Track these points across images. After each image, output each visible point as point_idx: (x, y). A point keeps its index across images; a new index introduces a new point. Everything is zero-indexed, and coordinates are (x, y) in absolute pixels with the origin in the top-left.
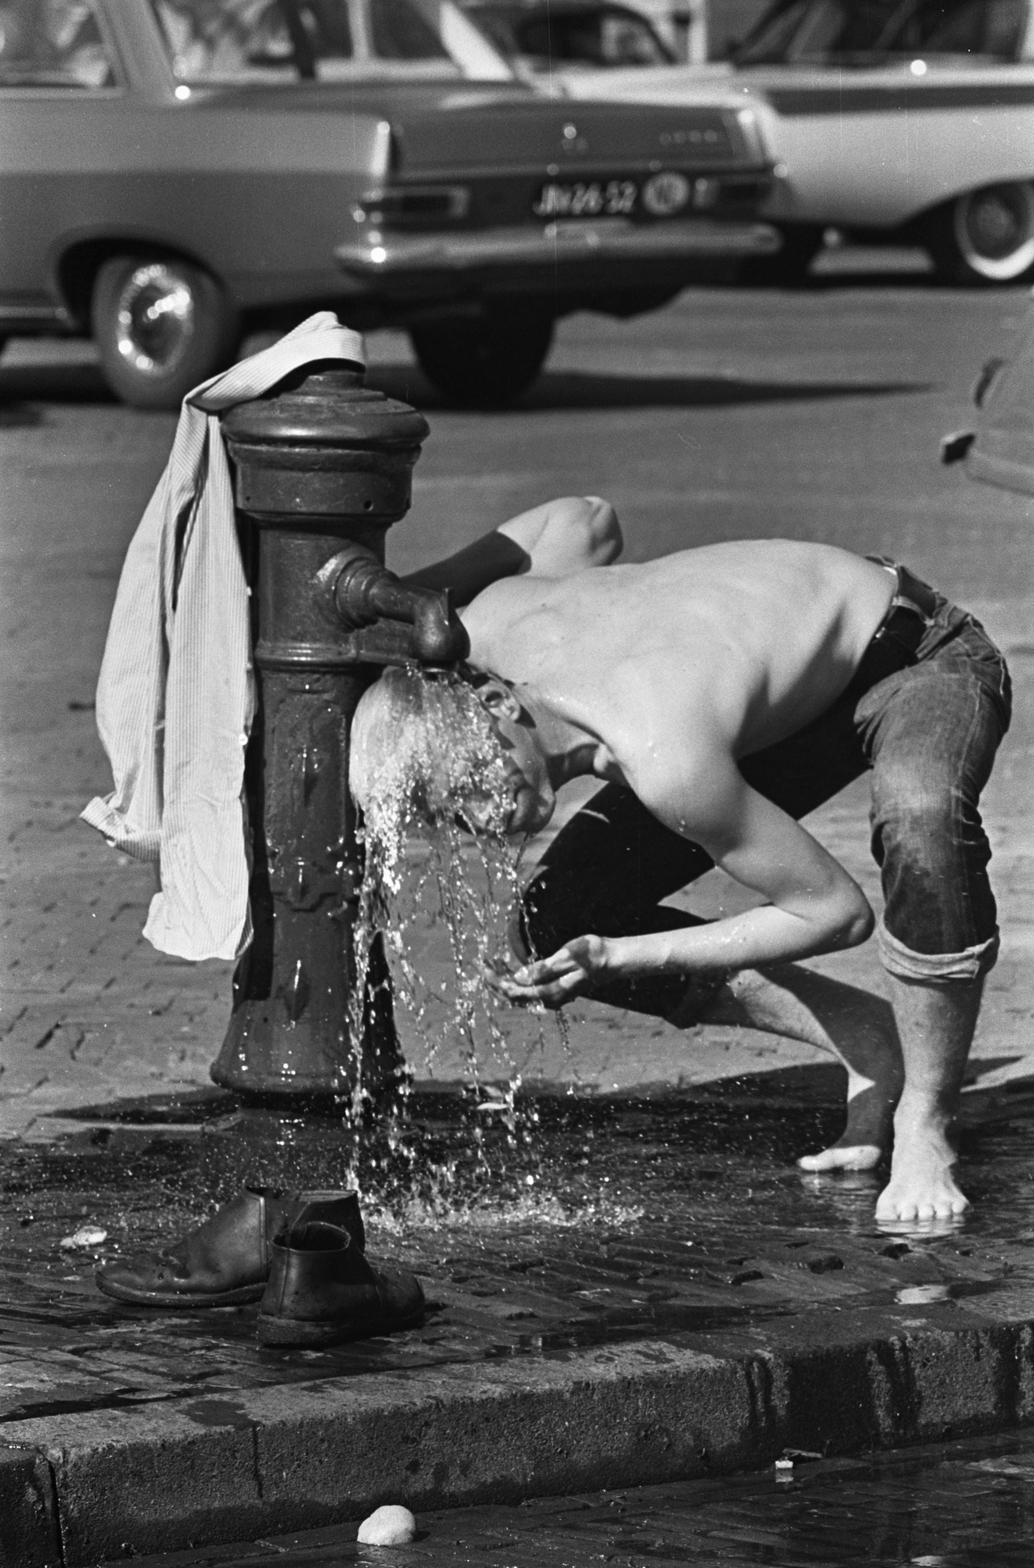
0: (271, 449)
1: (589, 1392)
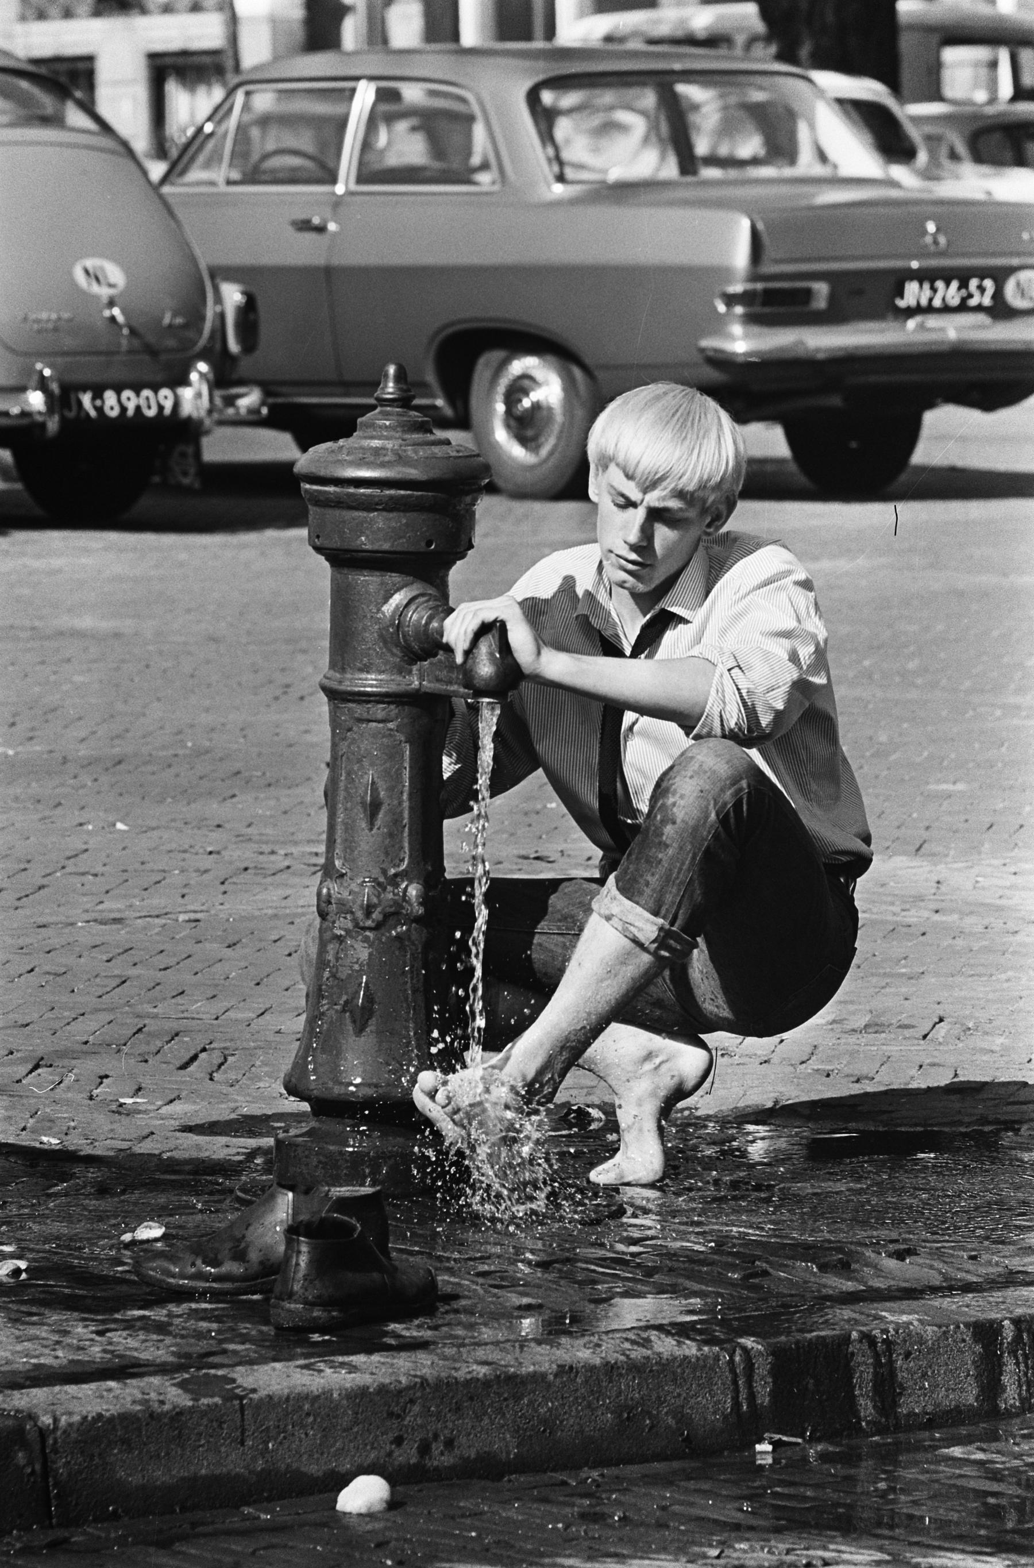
1: (573, 1375)
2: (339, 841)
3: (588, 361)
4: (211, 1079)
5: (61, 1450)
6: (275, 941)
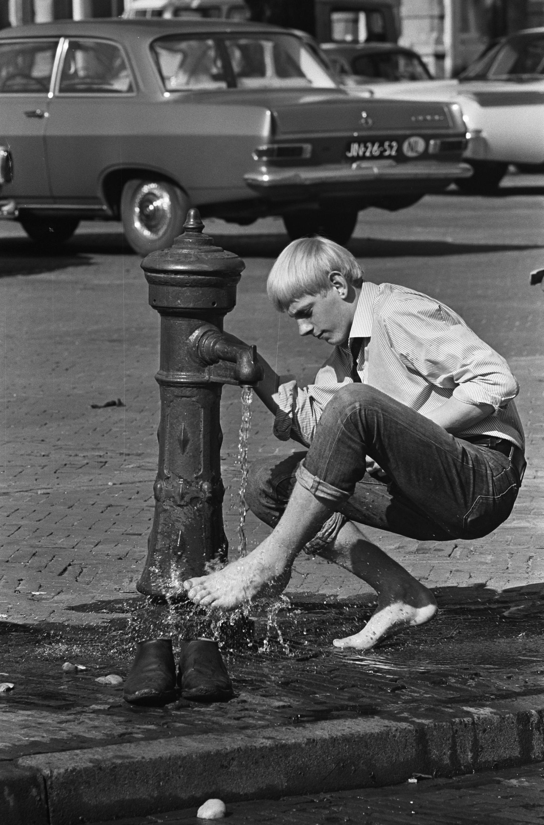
0: (165, 276)
1: (315, 744)
2: (166, 460)
3: (183, 184)
4: (77, 581)
5: (55, 788)
6: (93, 505)
